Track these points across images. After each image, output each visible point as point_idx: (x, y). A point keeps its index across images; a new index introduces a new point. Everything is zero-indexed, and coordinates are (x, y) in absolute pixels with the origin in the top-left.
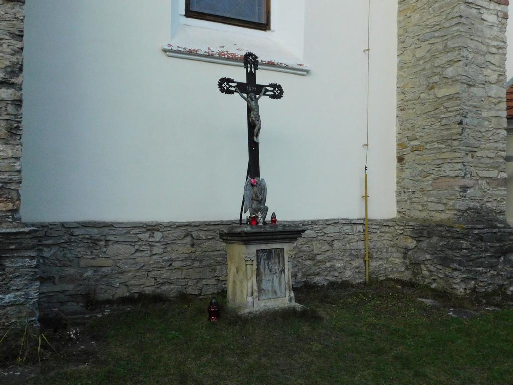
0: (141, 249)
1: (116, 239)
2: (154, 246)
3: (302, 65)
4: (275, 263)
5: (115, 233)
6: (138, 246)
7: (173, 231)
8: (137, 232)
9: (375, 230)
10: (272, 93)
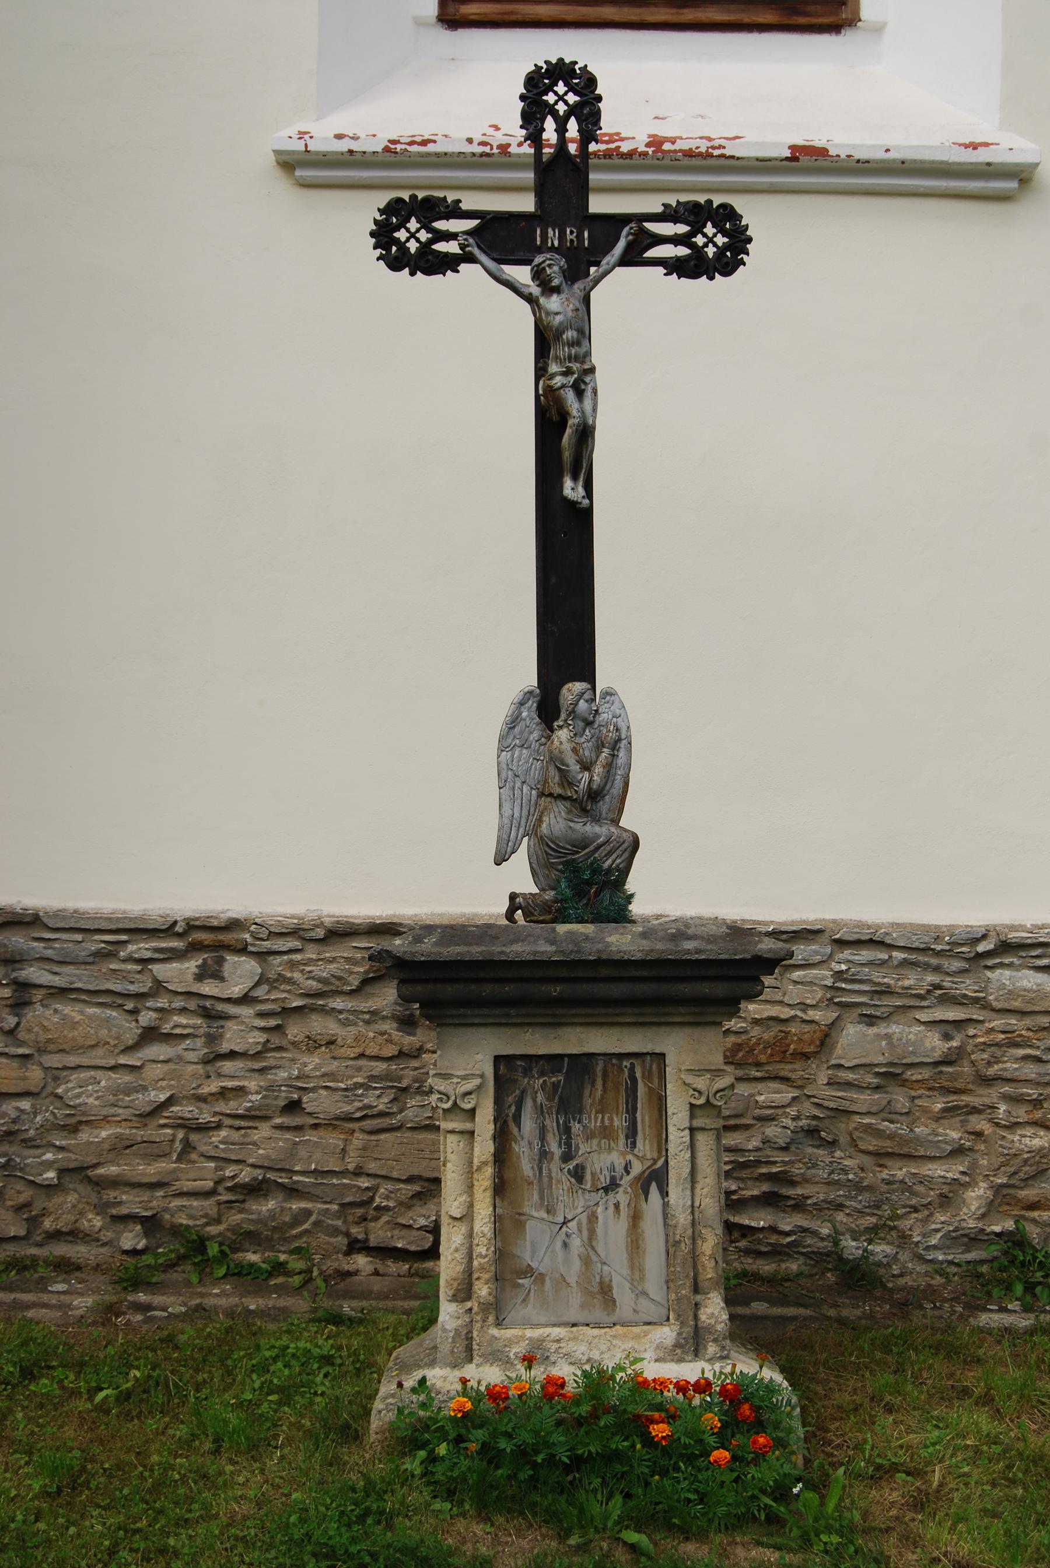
0: (166, 1028)
1: (57, 981)
2: (227, 1017)
3: (986, 145)
4: (606, 1133)
5: (49, 953)
6: (153, 1015)
7: (311, 952)
8: (148, 955)
10: (683, 251)
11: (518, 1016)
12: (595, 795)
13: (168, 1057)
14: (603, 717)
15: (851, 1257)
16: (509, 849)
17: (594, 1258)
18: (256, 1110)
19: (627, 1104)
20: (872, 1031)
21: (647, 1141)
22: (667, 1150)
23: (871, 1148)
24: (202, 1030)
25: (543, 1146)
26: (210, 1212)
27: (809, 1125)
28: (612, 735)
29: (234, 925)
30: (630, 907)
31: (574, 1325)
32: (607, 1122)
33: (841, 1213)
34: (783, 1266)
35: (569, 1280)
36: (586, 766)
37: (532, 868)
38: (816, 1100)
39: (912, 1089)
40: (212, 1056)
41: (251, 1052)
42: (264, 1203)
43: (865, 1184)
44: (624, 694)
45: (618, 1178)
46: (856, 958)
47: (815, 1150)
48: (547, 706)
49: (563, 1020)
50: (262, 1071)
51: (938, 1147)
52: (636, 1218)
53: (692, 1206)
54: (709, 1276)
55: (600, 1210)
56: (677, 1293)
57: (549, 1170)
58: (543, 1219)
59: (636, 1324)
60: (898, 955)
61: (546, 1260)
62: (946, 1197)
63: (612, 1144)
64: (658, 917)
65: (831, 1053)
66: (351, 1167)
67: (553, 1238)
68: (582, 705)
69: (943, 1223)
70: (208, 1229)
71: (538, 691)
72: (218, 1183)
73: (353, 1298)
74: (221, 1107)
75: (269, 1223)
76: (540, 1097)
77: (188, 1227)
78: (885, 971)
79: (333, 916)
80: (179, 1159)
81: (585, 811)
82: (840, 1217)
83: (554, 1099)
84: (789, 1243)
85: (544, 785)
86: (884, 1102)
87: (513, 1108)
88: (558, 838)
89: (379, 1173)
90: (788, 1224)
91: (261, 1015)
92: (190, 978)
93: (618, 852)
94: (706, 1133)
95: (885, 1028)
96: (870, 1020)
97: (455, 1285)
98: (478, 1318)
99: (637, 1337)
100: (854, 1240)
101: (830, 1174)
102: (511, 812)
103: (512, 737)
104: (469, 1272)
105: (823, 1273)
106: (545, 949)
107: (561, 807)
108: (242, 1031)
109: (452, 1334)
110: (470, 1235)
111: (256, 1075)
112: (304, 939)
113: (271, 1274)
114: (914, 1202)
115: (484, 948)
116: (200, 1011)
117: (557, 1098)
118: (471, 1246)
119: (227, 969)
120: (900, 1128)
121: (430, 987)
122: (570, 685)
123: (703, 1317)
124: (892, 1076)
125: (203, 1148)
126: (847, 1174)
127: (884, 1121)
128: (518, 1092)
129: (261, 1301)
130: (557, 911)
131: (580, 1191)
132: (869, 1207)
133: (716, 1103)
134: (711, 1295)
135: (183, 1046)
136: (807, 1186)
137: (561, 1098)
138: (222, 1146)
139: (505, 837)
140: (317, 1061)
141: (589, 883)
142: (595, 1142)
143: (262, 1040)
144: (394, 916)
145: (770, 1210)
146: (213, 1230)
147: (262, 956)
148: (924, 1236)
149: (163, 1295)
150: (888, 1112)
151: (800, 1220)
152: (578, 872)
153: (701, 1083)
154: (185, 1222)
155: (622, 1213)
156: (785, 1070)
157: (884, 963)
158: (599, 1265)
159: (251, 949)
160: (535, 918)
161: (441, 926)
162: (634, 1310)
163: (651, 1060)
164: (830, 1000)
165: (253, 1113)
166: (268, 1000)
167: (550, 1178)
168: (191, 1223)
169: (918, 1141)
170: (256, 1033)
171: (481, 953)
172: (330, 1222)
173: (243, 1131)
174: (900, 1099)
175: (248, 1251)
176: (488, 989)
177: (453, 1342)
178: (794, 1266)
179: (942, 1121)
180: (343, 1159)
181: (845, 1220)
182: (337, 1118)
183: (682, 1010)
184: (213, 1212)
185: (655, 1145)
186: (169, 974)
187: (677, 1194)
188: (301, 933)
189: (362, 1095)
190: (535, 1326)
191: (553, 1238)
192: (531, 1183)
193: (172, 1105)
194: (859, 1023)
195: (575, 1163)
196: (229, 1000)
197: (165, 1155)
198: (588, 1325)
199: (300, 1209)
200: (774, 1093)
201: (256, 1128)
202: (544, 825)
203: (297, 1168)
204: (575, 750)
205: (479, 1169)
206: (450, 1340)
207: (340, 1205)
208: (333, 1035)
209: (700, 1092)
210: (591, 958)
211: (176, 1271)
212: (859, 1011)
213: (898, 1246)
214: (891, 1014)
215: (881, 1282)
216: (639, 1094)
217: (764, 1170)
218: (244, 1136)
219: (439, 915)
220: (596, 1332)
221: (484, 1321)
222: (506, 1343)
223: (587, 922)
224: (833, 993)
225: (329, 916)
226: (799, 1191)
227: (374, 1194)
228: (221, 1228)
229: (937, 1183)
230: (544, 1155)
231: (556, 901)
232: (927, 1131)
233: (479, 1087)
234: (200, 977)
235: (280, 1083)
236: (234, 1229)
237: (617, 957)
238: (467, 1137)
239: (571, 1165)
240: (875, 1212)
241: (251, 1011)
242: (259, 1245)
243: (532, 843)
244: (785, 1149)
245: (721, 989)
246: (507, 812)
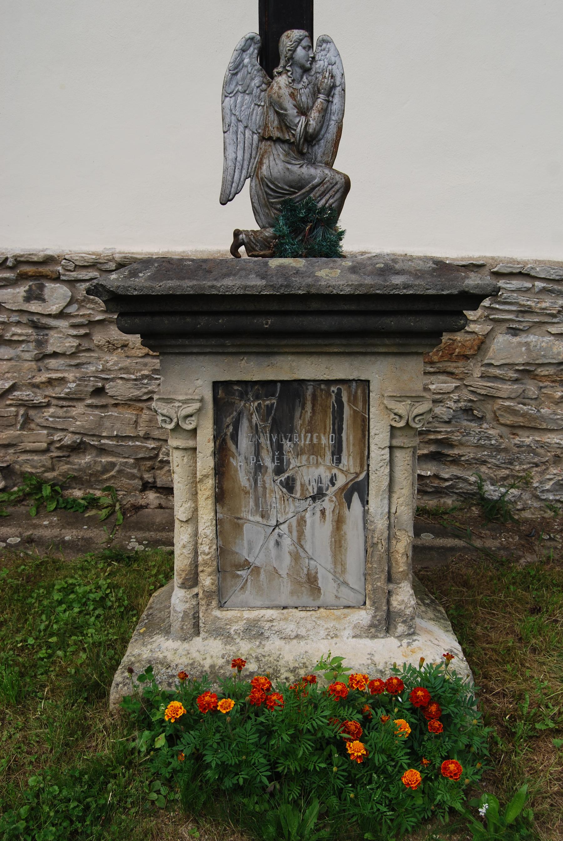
2: (51, 328)
4: (315, 450)
9: (246, 155)
11: (233, 346)
12: (311, 139)
13: (10, 356)
14: (320, 64)
15: (490, 497)
16: (233, 190)
17: (303, 554)
18: (72, 394)
19: (334, 424)
20: (516, 340)
21: (351, 458)
22: (368, 465)
23: (508, 422)
24: (33, 338)
25: (258, 460)
26: (46, 464)
27: (466, 406)
28: (328, 82)
29: (49, 260)
30: (341, 243)
31: (284, 608)
32: (315, 441)
33: (484, 467)
34: (442, 501)
35: (281, 572)
36: (303, 111)
37: (254, 207)
38: (472, 389)
39: (540, 381)
40: (41, 356)
41: (68, 353)
42: (83, 457)
43: (503, 447)
44: (339, 42)
45: (324, 488)
46: (508, 286)
47: (469, 423)
48: (267, 52)
49: (276, 350)
50: (77, 366)
51: (557, 423)
52: (339, 522)
53: (389, 512)
54: (401, 569)
55: (308, 515)
56: (373, 585)
57: (264, 481)
58: (258, 522)
59: (338, 608)
60: (539, 285)
61: (261, 555)
62: (559, 457)
63: (320, 460)
64: (363, 253)
65: (485, 356)
66: (141, 434)
67: (267, 538)
68: (300, 52)
69: (555, 474)
70: (46, 474)
71: (258, 38)
72: (51, 443)
73: (140, 529)
74: (50, 392)
75: (87, 471)
76: (255, 419)
77: (31, 473)
78: (528, 296)
79: (123, 253)
80: (22, 428)
81: (301, 154)
82: (484, 469)
83: (267, 420)
84: (447, 486)
85: (264, 130)
86: (520, 391)
87: (231, 428)
88: (276, 179)
89: (161, 438)
90: (447, 473)
91: (74, 326)
92: (21, 300)
93: (331, 192)
94: (404, 451)
95: (526, 337)
96: (515, 332)
97: (183, 576)
98: (203, 602)
99: (338, 618)
100: (492, 485)
101: (478, 440)
102: (234, 155)
103: (234, 83)
104: (195, 564)
105: (470, 508)
106: (255, 283)
107: (279, 150)
108: (61, 338)
109: (181, 615)
110: (196, 534)
111: (74, 369)
112: (101, 270)
113: (86, 508)
114: (536, 460)
115: (195, 282)
116: (30, 324)
117: (270, 419)
118: (196, 543)
119: (47, 293)
120: (530, 409)
121: (147, 319)
122: (289, 32)
123: (394, 603)
124: (527, 372)
125: (39, 421)
126: (490, 440)
127: (519, 404)
128: (235, 413)
129: (75, 532)
130: (275, 246)
131: (291, 499)
132: (504, 463)
133: (414, 425)
134: (402, 585)
135: (21, 349)
136: (462, 448)
137: (274, 419)
138: (51, 419)
139: (229, 178)
140: (116, 359)
141: (304, 221)
142: (304, 457)
143: (75, 344)
144: (168, 252)
145: (435, 463)
146: (49, 475)
147: (72, 283)
148: (541, 483)
149: (8, 526)
150: (523, 398)
151: (455, 471)
152: (295, 211)
153: (401, 408)
154: (29, 470)
155: (327, 518)
156: (451, 367)
157: (528, 290)
158: (307, 561)
159: (63, 278)
160: (256, 253)
161: (156, 260)
162: (336, 597)
163: (357, 386)
164: (487, 317)
165: (71, 396)
166: (78, 315)
167: (265, 488)
168: (34, 471)
169: (543, 418)
170: (71, 339)
171: (192, 287)
172: (129, 470)
173: (65, 409)
174: (532, 388)
175: (75, 488)
176: (203, 322)
177: (182, 621)
178: (449, 501)
179: (560, 404)
180: (136, 428)
181: (487, 471)
182: (131, 400)
183: (387, 341)
184: (48, 464)
185: (358, 461)
186: (6, 297)
187: (377, 504)
188: (99, 266)
189: (147, 384)
190: (252, 608)
191: (267, 538)
192: (248, 493)
193: (15, 390)
194: (506, 334)
195: (286, 475)
196: (49, 316)
197: (12, 425)
198: (296, 608)
199: (107, 462)
200: (442, 383)
201: (74, 407)
202: (264, 167)
203: (104, 434)
204: (292, 95)
205: (201, 481)
206: (180, 619)
207: (135, 459)
208: (126, 341)
209: (400, 417)
210: (300, 292)
211: (24, 505)
212: (507, 325)
213: (523, 489)
214: (530, 327)
215: (510, 515)
216: (345, 416)
217: (432, 437)
218: (66, 412)
219: (201, 252)
220: (303, 614)
221: (208, 605)
222: (227, 622)
223: (301, 256)
224: (489, 312)
225: (120, 253)
226: (456, 451)
227: (158, 452)
228: (55, 474)
229: (553, 448)
230: (259, 468)
231: (275, 237)
232: (549, 411)
233: (199, 410)
234: (28, 299)
235: (90, 375)
236: (64, 475)
237: (326, 292)
238: (189, 452)
239: (283, 477)
240: (509, 466)
241: (67, 324)
242: (83, 485)
243: (253, 184)
244: (448, 422)
245: (426, 323)
246: (231, 156)
